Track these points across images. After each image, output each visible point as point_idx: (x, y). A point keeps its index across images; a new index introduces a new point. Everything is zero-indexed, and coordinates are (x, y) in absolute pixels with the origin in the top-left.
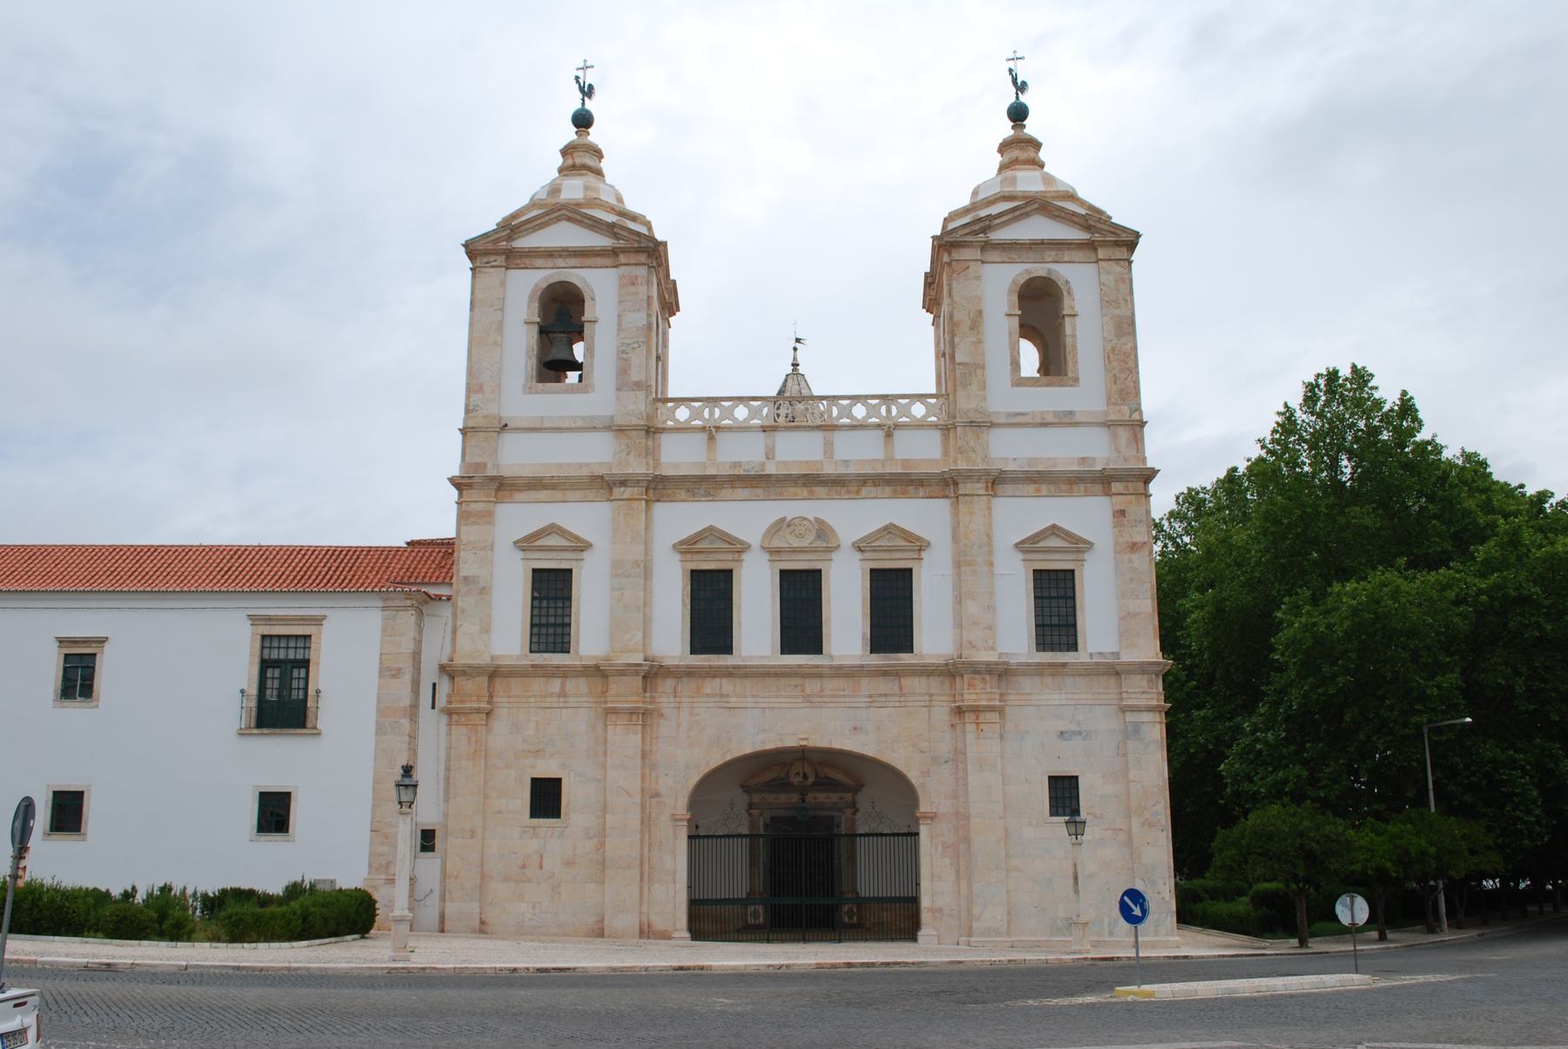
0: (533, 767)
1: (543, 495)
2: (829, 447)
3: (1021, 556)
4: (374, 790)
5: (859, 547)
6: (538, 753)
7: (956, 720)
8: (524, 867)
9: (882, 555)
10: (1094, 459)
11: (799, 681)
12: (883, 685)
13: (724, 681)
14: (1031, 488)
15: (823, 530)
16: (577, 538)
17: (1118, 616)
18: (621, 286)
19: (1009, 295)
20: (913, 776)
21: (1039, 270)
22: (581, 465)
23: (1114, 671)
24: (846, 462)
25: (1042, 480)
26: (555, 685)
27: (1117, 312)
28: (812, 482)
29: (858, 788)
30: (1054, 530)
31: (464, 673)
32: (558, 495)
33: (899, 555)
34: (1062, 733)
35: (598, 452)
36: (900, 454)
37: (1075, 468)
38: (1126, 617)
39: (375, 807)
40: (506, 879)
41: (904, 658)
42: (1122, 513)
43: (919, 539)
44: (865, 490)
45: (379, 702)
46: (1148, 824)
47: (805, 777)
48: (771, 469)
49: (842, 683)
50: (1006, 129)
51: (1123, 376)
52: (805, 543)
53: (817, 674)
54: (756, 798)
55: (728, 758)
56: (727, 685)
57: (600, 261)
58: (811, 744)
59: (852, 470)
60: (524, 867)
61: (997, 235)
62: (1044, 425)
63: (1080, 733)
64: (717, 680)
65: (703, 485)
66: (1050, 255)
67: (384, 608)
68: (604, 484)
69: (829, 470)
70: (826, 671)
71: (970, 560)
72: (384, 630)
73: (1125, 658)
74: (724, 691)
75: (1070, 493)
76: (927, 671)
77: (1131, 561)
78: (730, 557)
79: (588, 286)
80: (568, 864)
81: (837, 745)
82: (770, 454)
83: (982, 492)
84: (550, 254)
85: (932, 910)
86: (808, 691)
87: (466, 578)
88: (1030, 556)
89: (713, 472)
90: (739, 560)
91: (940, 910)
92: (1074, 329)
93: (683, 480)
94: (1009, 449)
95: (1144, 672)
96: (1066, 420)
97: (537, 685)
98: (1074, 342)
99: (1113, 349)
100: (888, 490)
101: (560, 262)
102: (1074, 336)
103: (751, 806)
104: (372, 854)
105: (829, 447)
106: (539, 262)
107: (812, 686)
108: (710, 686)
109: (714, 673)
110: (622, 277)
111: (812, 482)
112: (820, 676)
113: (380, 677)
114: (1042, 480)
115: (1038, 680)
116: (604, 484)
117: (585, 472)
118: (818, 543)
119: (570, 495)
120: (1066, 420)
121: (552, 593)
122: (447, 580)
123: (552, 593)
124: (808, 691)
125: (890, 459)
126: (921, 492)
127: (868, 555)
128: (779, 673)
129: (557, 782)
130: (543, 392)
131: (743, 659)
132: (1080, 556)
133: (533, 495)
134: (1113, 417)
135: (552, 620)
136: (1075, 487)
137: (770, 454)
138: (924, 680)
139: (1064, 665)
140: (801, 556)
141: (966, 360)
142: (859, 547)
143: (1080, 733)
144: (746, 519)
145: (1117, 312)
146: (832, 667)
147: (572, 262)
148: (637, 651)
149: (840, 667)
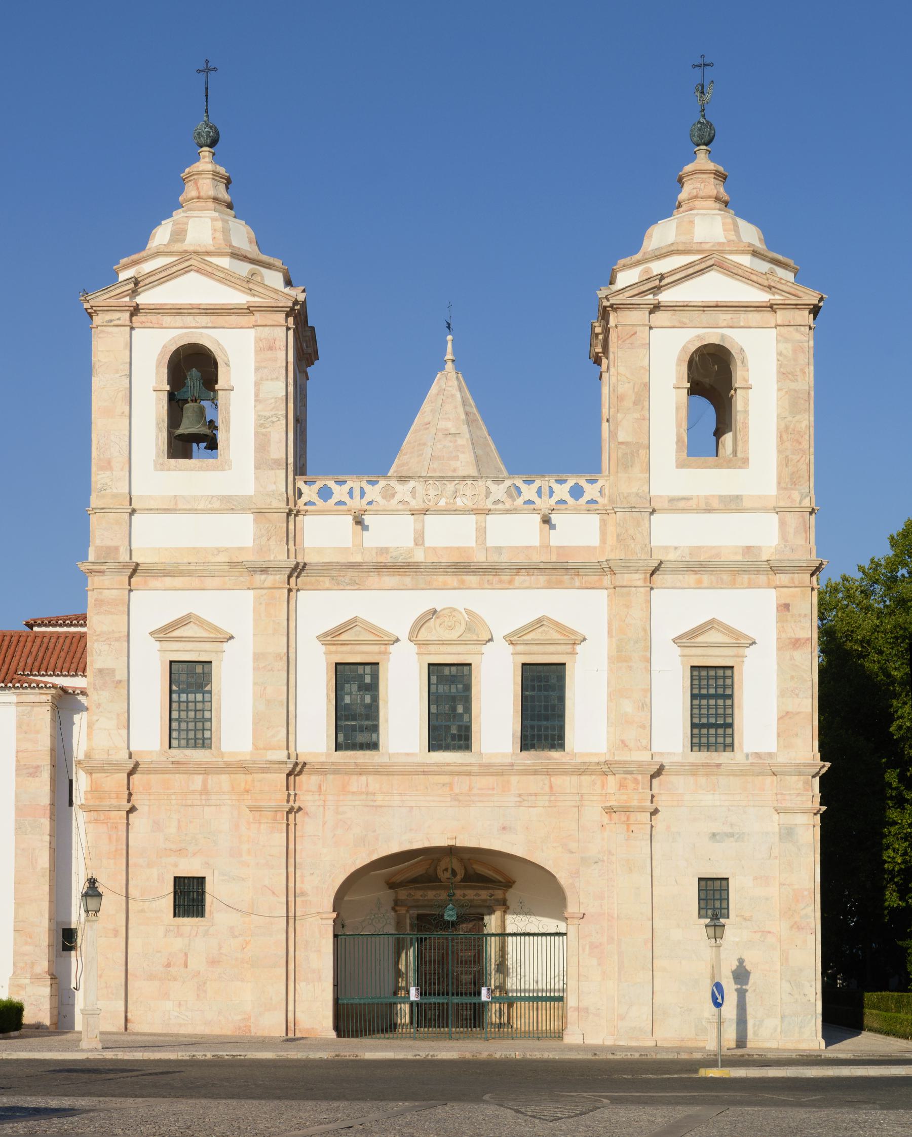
0: (176, 865)
1: (178, 581)
2: (482, 532)
3: (678, 651)
4: (16, 890)
5: (511, 639)
6: (180, 852)
7: (605, 819)
8: (168, 965)
9: (535, 648)
10: (759, 548)
11: (446, 779)
12: (536, 783)
13: (371, 778)
14: (691, 579)
15: (474, 621)
16: (216, 629)
17: (779, 710)
18: (259, 351)
19: (678, 365)
20: (562, 878)
21: (712, 337)
22: (219, 551)
23: (764, 766)
24: (499, 550)
25: (703, 568)
26: (197, 781)
27: (793, 386)
28: (462, 568)
29: (508, 884)
30: (711, 625)
31: (102, 770)
32: (195, 581)
33: (552, 648)
34: (714, 835)
35: (240, 534)
36: (557, 538)
37: (739, 558)
38: (785, 717)
39: (19, 904)
40: (151, 977)
41: (723, 757)
42: (786, 607)
43: (574, 632)
44: (519, 579)
45: (17, 801)
46: (797, 927)
47: (454, 873)
48: (419, 556)
49: (491, 780)
50: (698, 117)
51: (796, 458)
52: (454, 635)
53: (206, 770)
54: (403, 894)
55: (375, 857)
56: (373, 782)
57: (233, 319)
58: (459, 844)
59: (504, 558)
60: (168, 965)
61: (665, 297)
62: (709, 510)
63: (731, 835)
64: (364, 778)
65: (350, 572)
66: (725, 317)
67: (18, 704)
68: (240, 570)
69: (480, 557)
70: (475, 769)
71: (631, 652)
72: (19, 726)
73: (781, 759)
74: (371, 789)
75: (733, 585)
76: (583, 770)
77: (792, 658)
78: (376, 648)
79: (223, 350)
80: (213, 962)
81: (485, 845)
82: (419, 539)
83: (640, 583)
84: (178, 310)
85: (578, 1009)
86: (457, 790)
87: (100, 671)
88: (688, 651)
89: (358, 559)
90: (386, 653)
91: (586, 1010)
92: (746, 404)
93: (326, 568)
94: (670, 534)
95: (800, 774)
96: (732, 504)
97: (178, 780)
98: (746, 418)
99: (787, 428)
100: (542, 579)
101: (189, 320)
102: (746, 412)
103: (397, 903)
104: (16, 953)
105: (482, 532)
106: (167, 320)
107: (461, 784)
108: (356, 783)
109: (361, 770)
110: (258, 340)
111: (462, 568)
112: (469, 774)
113: (17, 775)
114: (703, 568)
115: (691, 779)
116: (240, 570)
117: (223, 558)
118: (468, 636)
119: (209, 582)
120: (732, 504)
121: (190, 682)
122: (79, 669)
123: (190, 682)
124: (457, 790)
125: (546, 547)
126: (577, 581)
127: (520, 648)
128: (425, 771)
129: (201, 881)
130: (176, 469)
131: (390, 756)
132: (740, 651)
133: (168, 581)
134: (782, 504)
135: (712, 691)
136: (739, 579)
137: (419, 539)
138: (575, 778)
139: (718, 766)
140: (449, 649)
141: (629, 439)
142: (511, 639)
143: (731, 835)
144: (390, 610)
145: (793, 386)
146: (481, 765)
147: (204, 320)
148: (280, 749)
149: (489, 766)
